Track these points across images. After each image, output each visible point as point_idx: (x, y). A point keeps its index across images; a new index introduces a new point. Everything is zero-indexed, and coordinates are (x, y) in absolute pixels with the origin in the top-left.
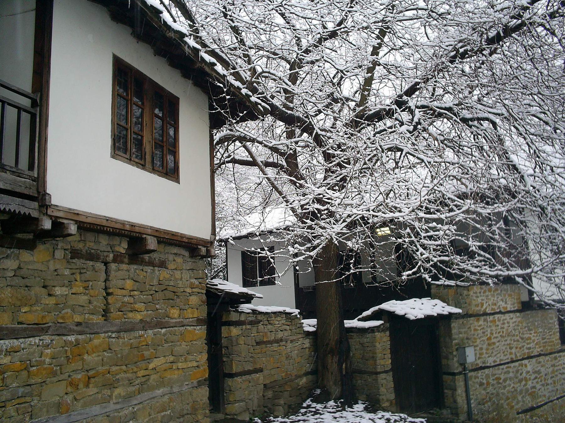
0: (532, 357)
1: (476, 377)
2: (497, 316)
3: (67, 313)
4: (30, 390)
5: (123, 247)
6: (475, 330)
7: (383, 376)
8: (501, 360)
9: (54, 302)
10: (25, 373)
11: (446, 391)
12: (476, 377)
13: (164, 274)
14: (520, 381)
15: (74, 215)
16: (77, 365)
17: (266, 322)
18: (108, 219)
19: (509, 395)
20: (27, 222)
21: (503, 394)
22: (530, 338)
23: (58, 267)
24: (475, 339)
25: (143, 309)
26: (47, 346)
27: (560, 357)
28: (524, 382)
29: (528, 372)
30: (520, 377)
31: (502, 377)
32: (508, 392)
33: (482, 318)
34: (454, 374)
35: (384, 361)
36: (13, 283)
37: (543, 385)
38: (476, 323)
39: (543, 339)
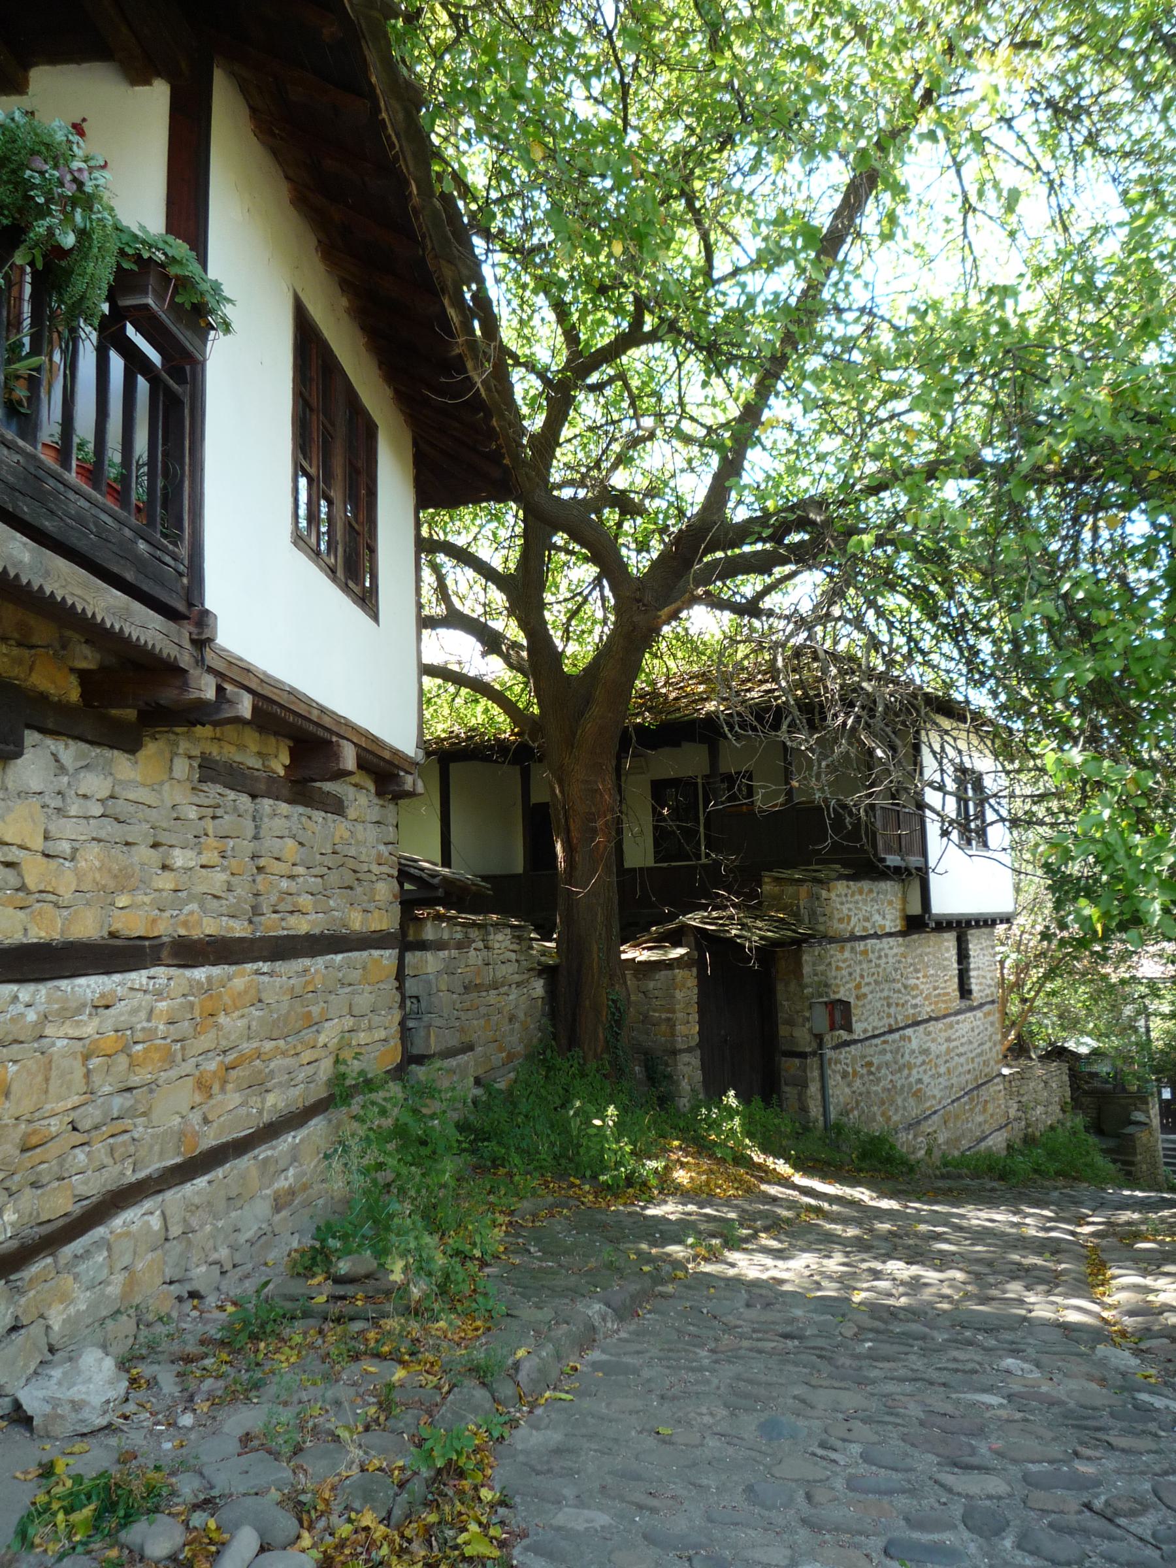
0: (917, 1023)
1: (838, 1062)
2: (870, 942)
3: (192, 913)
4: (132, 1102)
5: (280, 763)
6: (838, 968)
7: (685, 1058)
8: (875, 1028)
9: (172, 886)
10: (122, 1060)
11: (787, 1089)
12: (838, 1062)
13: (339, 828)
14: (900, 1070)
15: (236, 674)
16: (206, 1041)
17: (480, 945)
18: (292, 692)
19: (884, 1096)
20: (173, 671)
21: (876, 1093)
22: (916, 986)
23: (178, 799)
24: (837, 986)
25: (310, 908)
26: (159, 994)
27: (958, 1023)
28: (906, 1072)
29: (913, 1052)
30: (901, 1061)
31: (875, 1061)
32: (884, 1089)
33: (849, 945)
34: (803, 1055)
35: (688, 1029)
36: (102, 834)
37: (932, 1076)
38: (839, 956)
39: (935, 989)
